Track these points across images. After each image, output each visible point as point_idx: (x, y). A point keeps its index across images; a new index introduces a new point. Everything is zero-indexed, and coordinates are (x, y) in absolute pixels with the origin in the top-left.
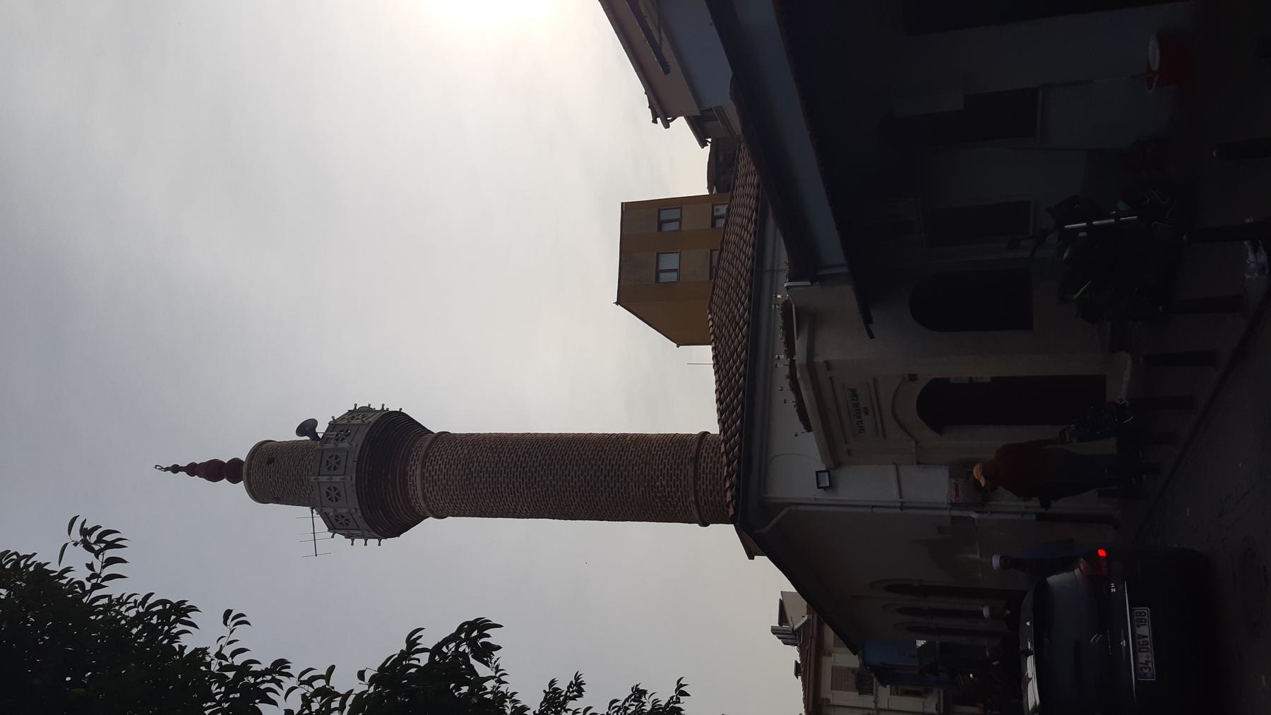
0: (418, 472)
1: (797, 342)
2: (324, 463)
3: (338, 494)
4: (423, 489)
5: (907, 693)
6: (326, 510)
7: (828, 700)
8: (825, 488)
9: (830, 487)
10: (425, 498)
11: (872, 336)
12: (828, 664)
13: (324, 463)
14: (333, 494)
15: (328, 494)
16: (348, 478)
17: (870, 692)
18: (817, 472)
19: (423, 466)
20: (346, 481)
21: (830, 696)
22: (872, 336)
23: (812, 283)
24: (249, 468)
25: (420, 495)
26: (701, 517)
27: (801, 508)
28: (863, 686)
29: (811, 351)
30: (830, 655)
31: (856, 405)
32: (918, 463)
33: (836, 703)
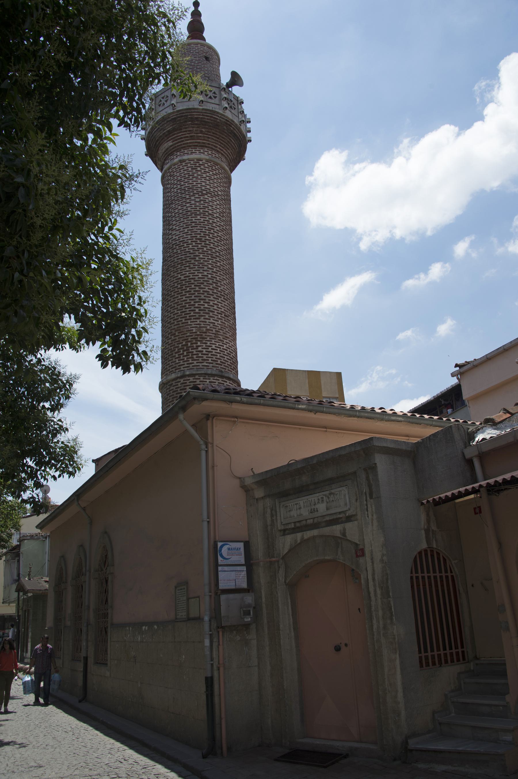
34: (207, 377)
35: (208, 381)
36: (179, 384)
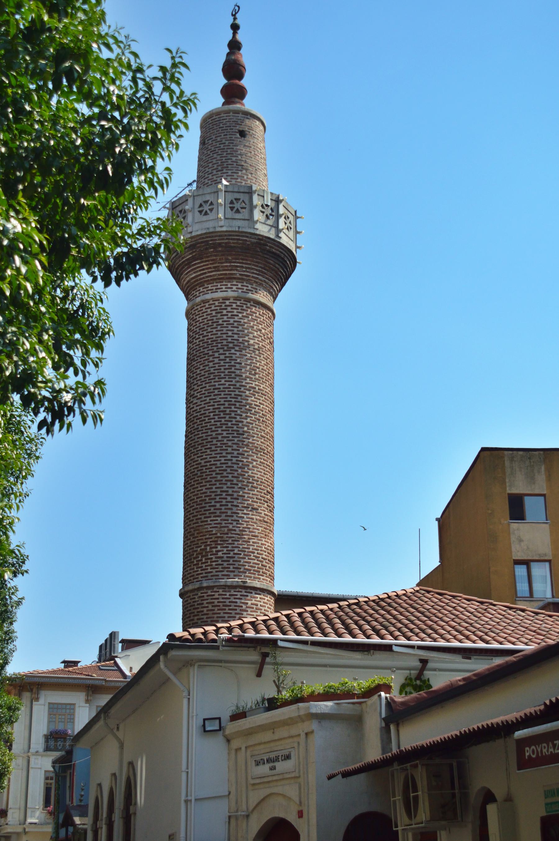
0: (230, 294)
1: (330, 704)
2: (237, 196)
3: (206, 213)
4: (214, 300)
5: (48, 790)
6: (190, 201)
7: (37, 699)
8: (204, 726)
9: (205, 731)
10: (204, 302)
11: (330, 777)
12: (77, 699)
13: (237, 196)
14: (206, 208)
15: (206, 202)
16: (222, 223)
17: (47, 749)
18: (219, 719)
19: (237, 299)
20: (221, 220)
21: (42, 701)
22: (330, 777)
23: (384, 719)
24: (237, 112)
25: (208, 297)
26: (187, 592)
27: (185, 701)
28: (54, 738)
29: (321, 717)
30: (87, 701)
31: (277, 759)
32: (230, 817)
33: (35, 708)
34: (227, 590)
35: (228, 594)
36: (196, 597)
